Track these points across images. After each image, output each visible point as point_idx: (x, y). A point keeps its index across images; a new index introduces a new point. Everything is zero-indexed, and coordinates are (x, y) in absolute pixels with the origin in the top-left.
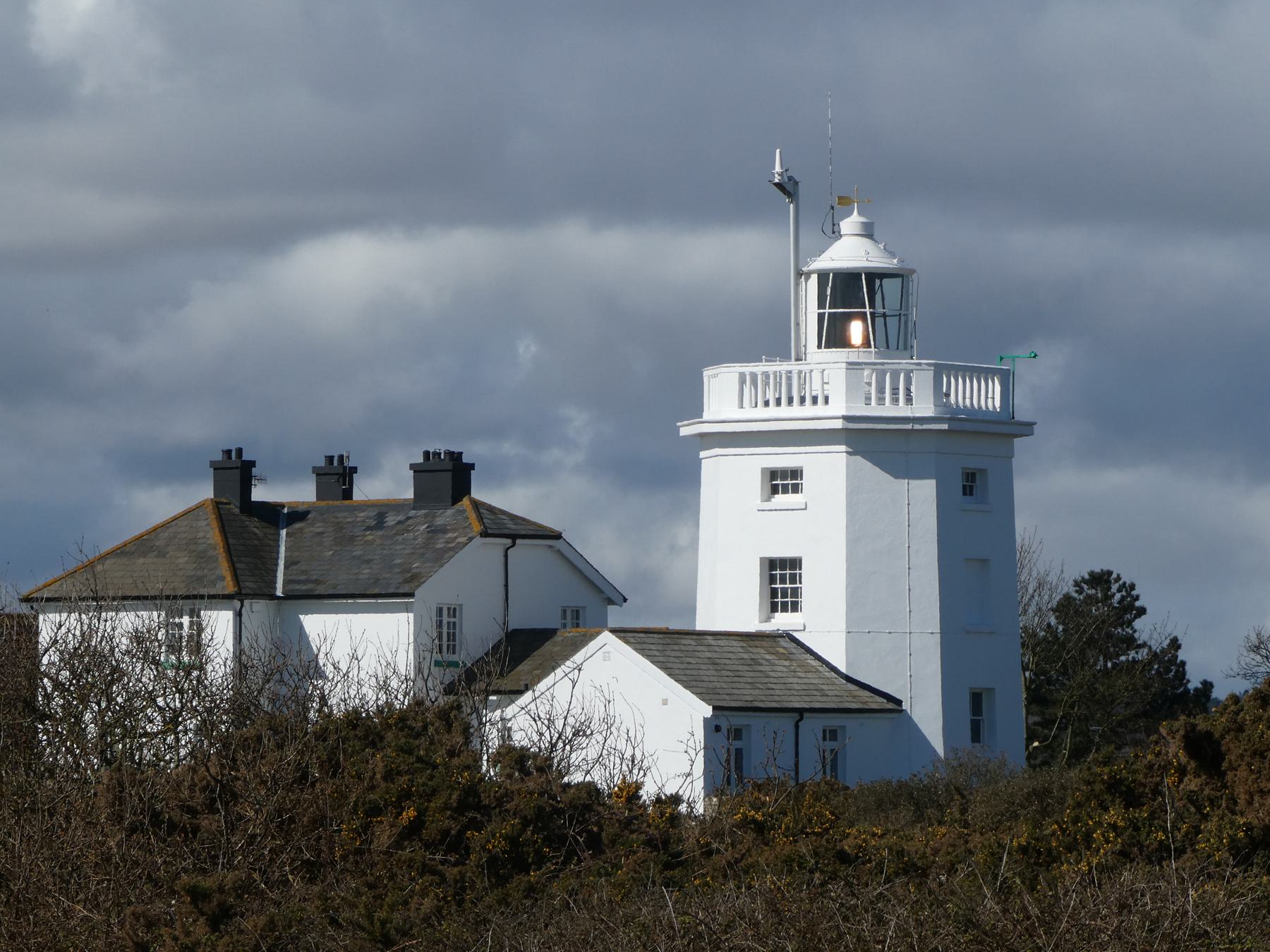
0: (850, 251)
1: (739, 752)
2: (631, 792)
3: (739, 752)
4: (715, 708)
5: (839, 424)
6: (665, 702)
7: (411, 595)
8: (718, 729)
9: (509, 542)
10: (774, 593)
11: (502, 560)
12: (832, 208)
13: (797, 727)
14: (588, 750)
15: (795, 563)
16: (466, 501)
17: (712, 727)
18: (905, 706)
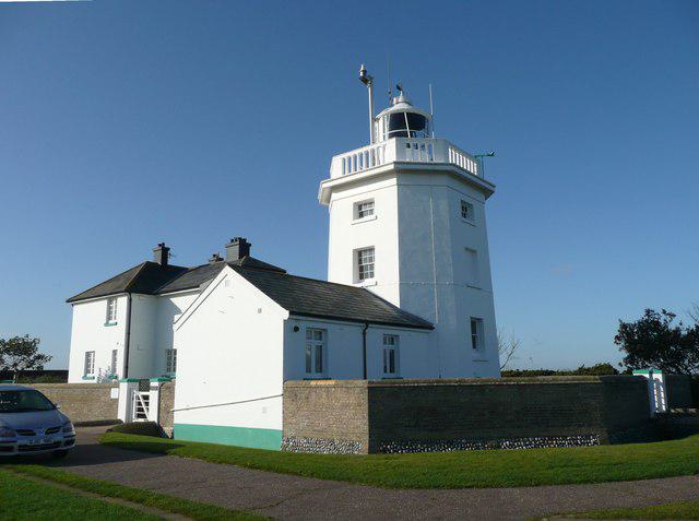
0: (399, 105)
1: (392, 353)
3: (392, 353)
5: (392, 167)
6: (260, 311)
10: (361, 269)
11: (362, 338)
13: (364, 334)
14: (103, 371)
15: (371, 250)
17: (291, 329)
18: (436, 321)
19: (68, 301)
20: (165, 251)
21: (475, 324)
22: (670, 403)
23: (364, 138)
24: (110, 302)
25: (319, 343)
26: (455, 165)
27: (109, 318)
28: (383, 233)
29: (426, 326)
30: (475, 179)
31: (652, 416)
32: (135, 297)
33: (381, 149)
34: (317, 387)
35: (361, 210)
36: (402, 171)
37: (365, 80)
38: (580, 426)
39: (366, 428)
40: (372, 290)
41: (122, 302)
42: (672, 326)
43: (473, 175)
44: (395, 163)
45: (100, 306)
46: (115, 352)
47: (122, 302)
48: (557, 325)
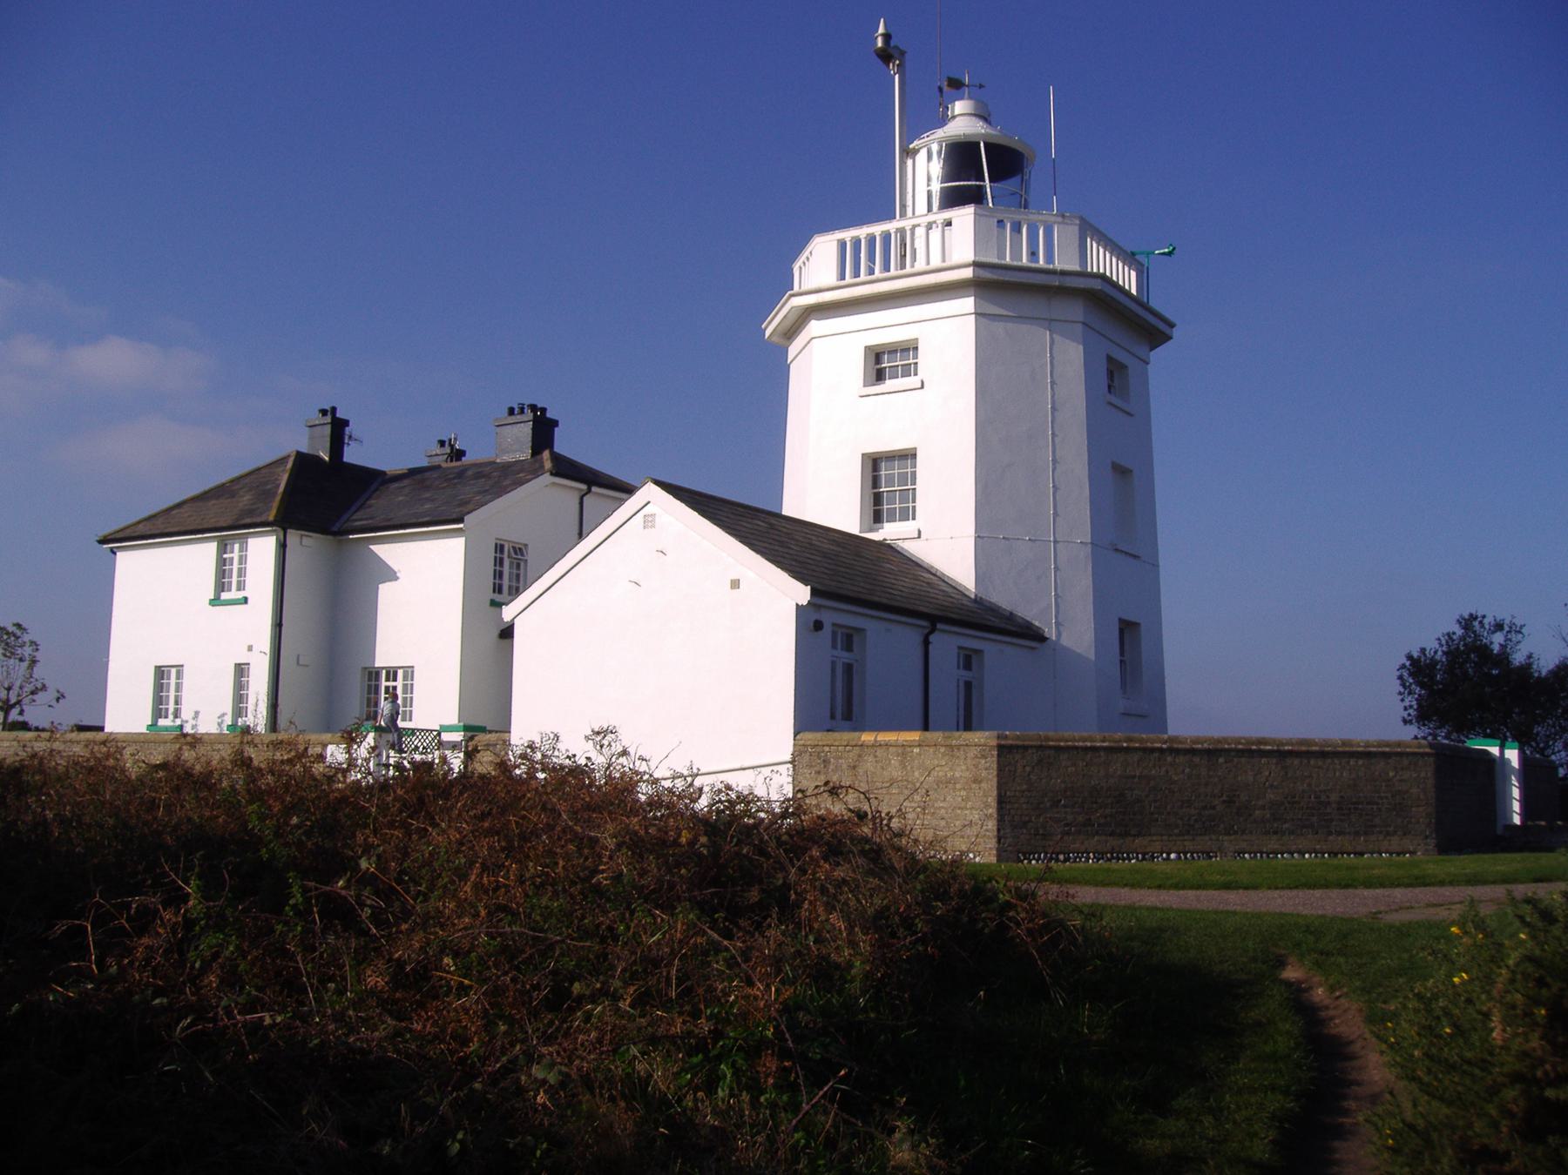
0: (962, 121)
1: (848, 669)
2: (1341, 1133)
4: (814, 592)
5: (968, 273)
6: (735, 584)
7: (460, 520)
8: (818, 626)
9: (584, 487)
10: (878, 499)
11: (577, 506)
12: (941, 90)
13: (926, 643)
15: (909, 456)
16: (546, 454)
17: (809, 623)
18: (1051, 632)
19: (103, 541)
20: (339, 428)
21: (1127, 628)
22: (1525, 813)
23: (879, 200)
24: (223, 548)
25: (846, 657)
26: (1103, 277)
27: (221, 586)
28: (938, 417)
29: (1029, 634)
30: (1133, 306)
31: (1499, 831)
32: (293, 537)
33: (920, 232)
34: (876, 745)
35: (883, 364)
36: (994, 286)
37: (885, 56)
38: (1388, 834)
39: (992, 825)
40: (914, 549)
41: (261, 550)
42: (1518, 658)
43: (1127, 294)
44: (976, 264)
45: (200, 556)
46: (241, 670)
47: (261, 550)
48: (1290, 642)
